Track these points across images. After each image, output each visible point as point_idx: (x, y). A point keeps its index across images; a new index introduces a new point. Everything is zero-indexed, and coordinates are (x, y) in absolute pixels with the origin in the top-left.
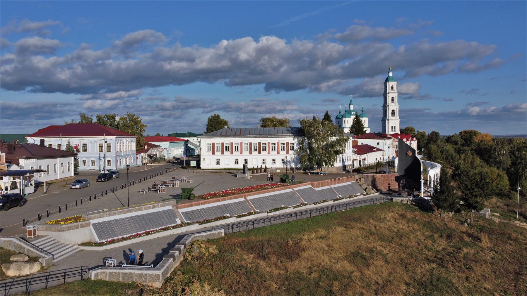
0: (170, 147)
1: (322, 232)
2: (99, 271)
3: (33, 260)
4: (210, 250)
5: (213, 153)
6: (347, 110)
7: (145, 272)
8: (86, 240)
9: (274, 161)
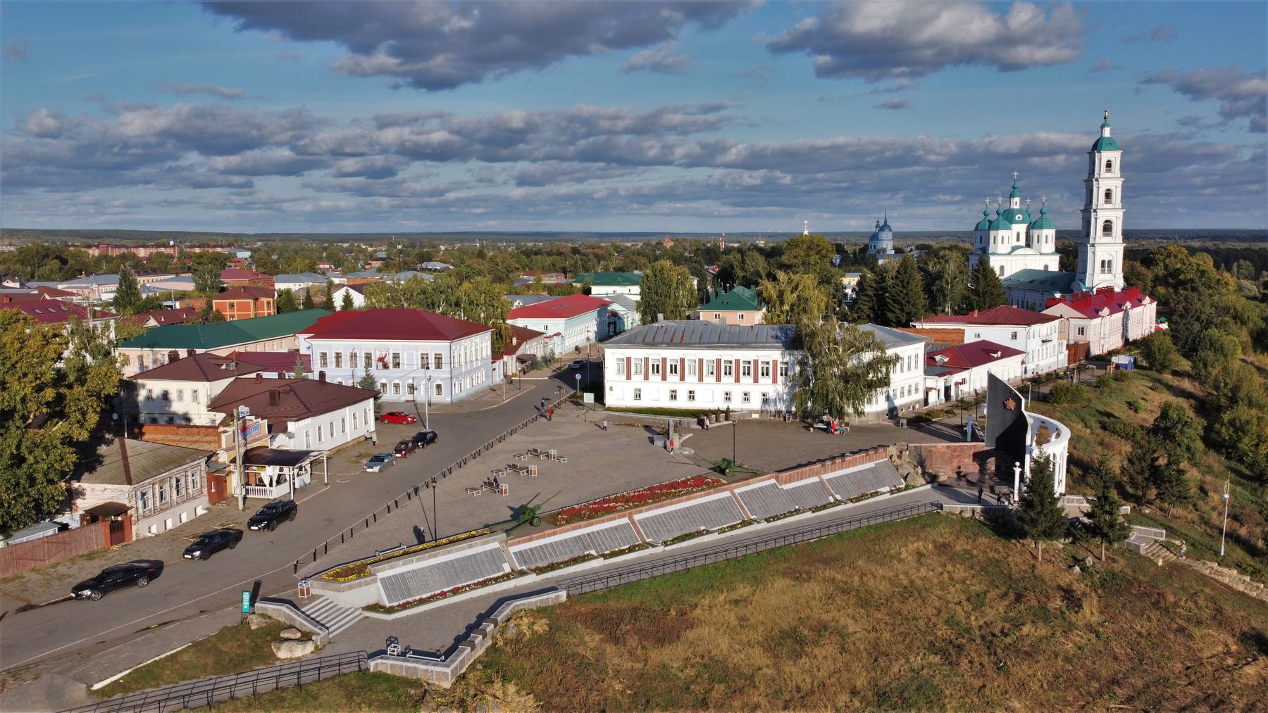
0: (566, 328)
1: (743, 590)
2: (380, 661)
3: (306, 637)
4: (536, 627)
5: (629, 377)
6: (1001, 211)
7: (431, 668)
8: (372, 601)
9: (746, 397)
